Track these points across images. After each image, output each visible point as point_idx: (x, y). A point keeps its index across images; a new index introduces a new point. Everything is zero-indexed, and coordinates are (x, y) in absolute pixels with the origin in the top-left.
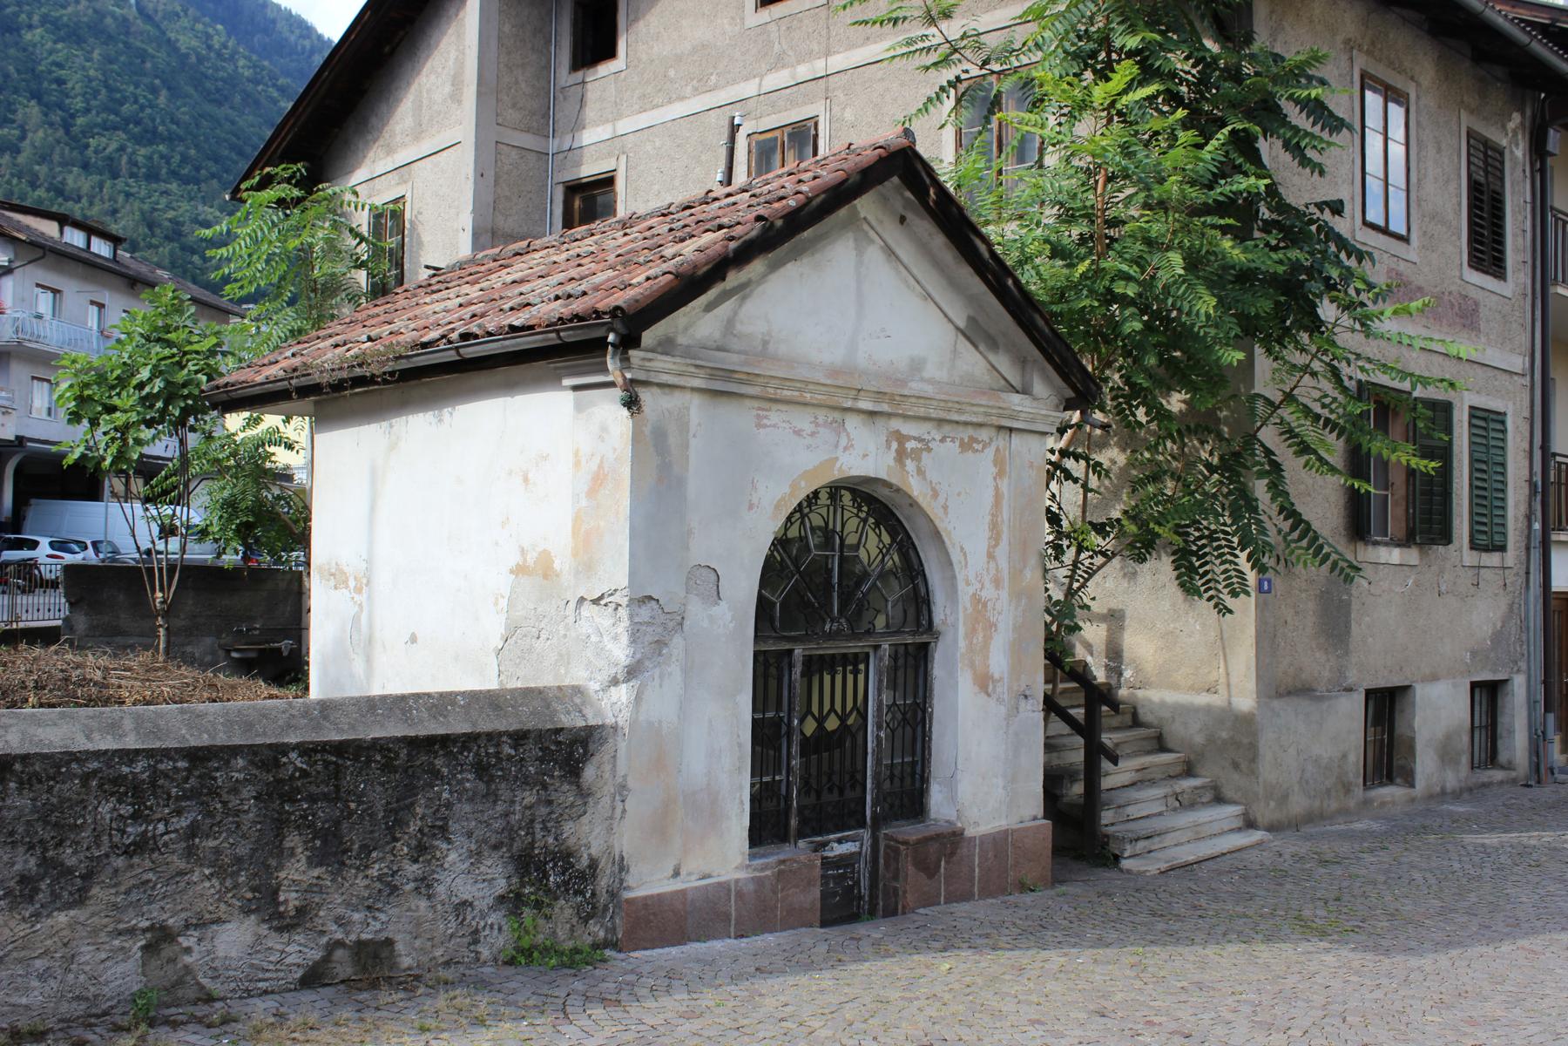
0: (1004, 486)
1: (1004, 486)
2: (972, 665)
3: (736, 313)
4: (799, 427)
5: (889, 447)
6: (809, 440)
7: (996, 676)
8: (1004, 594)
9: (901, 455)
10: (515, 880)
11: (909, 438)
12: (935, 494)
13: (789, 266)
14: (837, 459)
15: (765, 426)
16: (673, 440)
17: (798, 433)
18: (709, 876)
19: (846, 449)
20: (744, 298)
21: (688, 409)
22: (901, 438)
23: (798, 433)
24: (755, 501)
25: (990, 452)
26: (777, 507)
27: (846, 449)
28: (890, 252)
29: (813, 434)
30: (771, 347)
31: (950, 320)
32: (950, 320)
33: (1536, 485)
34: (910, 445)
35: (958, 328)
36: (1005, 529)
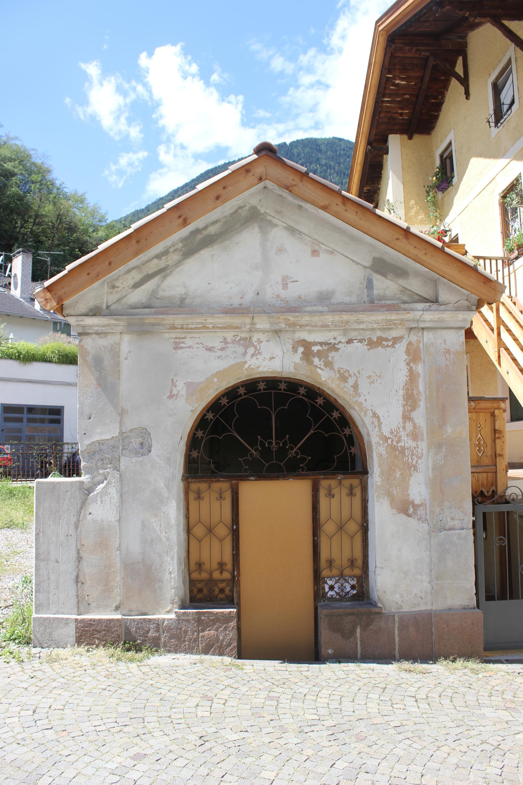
0: (420, 368)
1: (420, 368)
2: (389, 495)
3: (159, 286)
4: (210, 345)
5: (296, 351)
6: (219, 353)
7: (417, 502)
8: (423, 446)
9: (308, 355)
10: (415, 392)
11: (315, 344)
12: (344, 378)
13: (202, 252)
14: (246, 362)
15: (182, 348)
16: (107, 362)
17: (210, 349)
18: (145, 614)
19: (253, 355)
20: (165, 277)
21: (119, 344)
22: (307, 345)
23: (210, 349)
24: (175, 392)
25: (401, 347)
26: (217, 389)
27: (253, 355)
28: (292, 230)
29: (222, 349)
30: (187, 301)
31: (357, 263)
32: (357, 263)
33: (194, 188)
34: (315, 348)
35: (365, 267)
36: (423, 398)
